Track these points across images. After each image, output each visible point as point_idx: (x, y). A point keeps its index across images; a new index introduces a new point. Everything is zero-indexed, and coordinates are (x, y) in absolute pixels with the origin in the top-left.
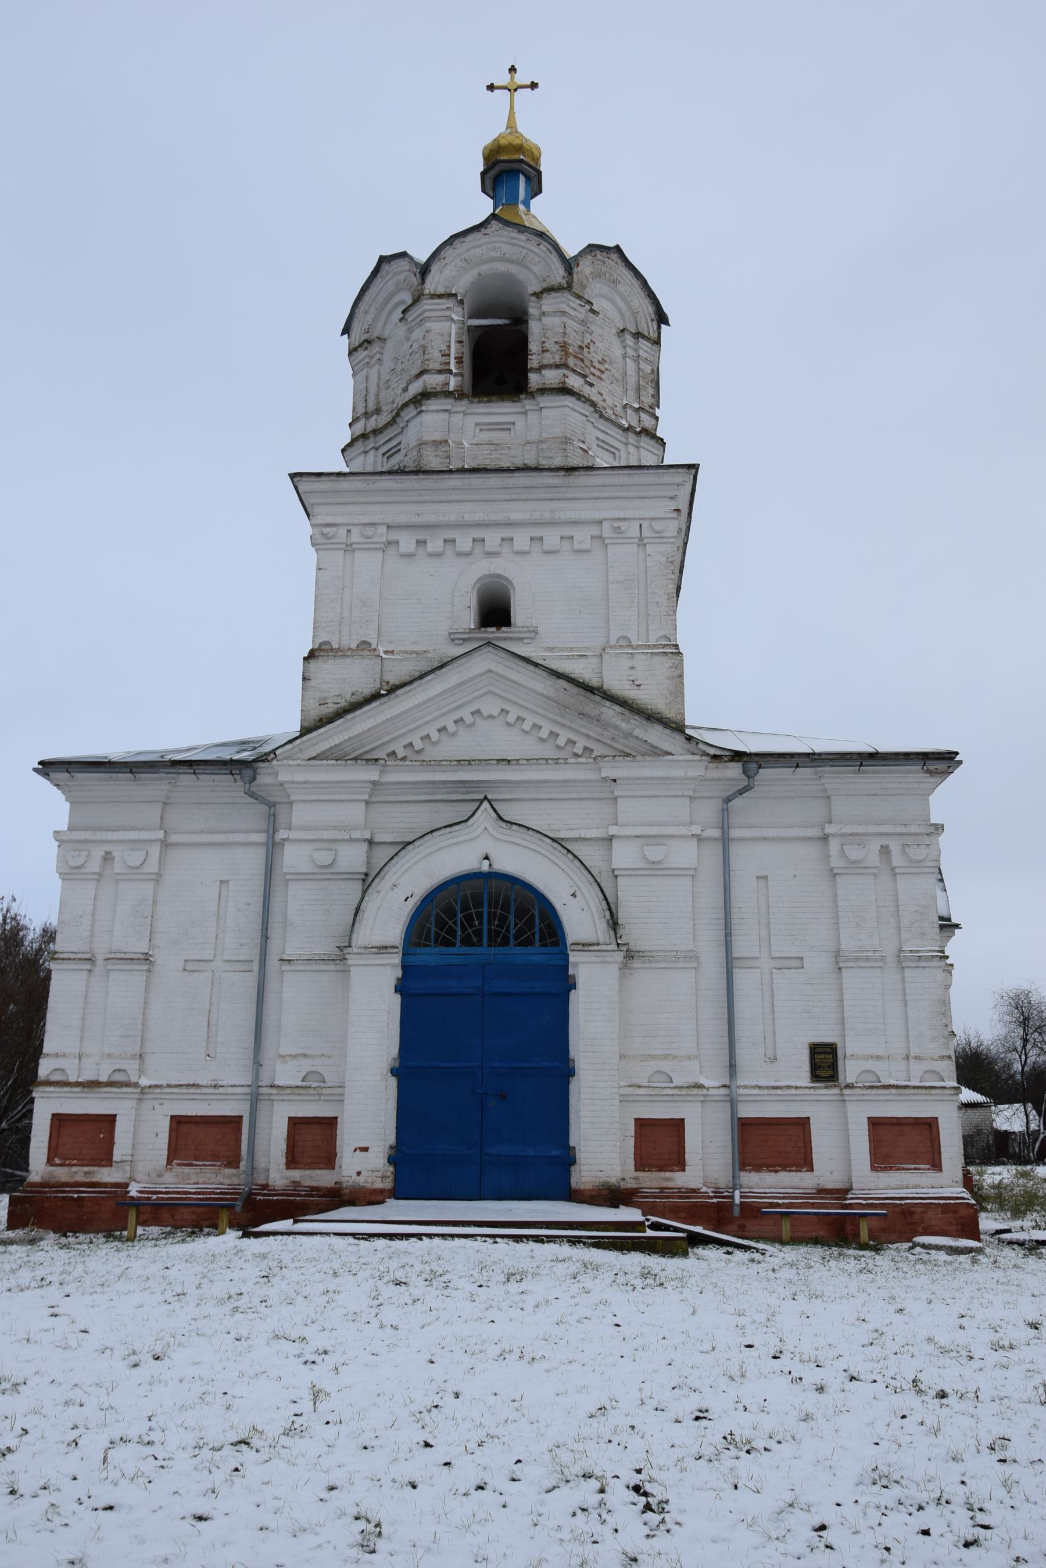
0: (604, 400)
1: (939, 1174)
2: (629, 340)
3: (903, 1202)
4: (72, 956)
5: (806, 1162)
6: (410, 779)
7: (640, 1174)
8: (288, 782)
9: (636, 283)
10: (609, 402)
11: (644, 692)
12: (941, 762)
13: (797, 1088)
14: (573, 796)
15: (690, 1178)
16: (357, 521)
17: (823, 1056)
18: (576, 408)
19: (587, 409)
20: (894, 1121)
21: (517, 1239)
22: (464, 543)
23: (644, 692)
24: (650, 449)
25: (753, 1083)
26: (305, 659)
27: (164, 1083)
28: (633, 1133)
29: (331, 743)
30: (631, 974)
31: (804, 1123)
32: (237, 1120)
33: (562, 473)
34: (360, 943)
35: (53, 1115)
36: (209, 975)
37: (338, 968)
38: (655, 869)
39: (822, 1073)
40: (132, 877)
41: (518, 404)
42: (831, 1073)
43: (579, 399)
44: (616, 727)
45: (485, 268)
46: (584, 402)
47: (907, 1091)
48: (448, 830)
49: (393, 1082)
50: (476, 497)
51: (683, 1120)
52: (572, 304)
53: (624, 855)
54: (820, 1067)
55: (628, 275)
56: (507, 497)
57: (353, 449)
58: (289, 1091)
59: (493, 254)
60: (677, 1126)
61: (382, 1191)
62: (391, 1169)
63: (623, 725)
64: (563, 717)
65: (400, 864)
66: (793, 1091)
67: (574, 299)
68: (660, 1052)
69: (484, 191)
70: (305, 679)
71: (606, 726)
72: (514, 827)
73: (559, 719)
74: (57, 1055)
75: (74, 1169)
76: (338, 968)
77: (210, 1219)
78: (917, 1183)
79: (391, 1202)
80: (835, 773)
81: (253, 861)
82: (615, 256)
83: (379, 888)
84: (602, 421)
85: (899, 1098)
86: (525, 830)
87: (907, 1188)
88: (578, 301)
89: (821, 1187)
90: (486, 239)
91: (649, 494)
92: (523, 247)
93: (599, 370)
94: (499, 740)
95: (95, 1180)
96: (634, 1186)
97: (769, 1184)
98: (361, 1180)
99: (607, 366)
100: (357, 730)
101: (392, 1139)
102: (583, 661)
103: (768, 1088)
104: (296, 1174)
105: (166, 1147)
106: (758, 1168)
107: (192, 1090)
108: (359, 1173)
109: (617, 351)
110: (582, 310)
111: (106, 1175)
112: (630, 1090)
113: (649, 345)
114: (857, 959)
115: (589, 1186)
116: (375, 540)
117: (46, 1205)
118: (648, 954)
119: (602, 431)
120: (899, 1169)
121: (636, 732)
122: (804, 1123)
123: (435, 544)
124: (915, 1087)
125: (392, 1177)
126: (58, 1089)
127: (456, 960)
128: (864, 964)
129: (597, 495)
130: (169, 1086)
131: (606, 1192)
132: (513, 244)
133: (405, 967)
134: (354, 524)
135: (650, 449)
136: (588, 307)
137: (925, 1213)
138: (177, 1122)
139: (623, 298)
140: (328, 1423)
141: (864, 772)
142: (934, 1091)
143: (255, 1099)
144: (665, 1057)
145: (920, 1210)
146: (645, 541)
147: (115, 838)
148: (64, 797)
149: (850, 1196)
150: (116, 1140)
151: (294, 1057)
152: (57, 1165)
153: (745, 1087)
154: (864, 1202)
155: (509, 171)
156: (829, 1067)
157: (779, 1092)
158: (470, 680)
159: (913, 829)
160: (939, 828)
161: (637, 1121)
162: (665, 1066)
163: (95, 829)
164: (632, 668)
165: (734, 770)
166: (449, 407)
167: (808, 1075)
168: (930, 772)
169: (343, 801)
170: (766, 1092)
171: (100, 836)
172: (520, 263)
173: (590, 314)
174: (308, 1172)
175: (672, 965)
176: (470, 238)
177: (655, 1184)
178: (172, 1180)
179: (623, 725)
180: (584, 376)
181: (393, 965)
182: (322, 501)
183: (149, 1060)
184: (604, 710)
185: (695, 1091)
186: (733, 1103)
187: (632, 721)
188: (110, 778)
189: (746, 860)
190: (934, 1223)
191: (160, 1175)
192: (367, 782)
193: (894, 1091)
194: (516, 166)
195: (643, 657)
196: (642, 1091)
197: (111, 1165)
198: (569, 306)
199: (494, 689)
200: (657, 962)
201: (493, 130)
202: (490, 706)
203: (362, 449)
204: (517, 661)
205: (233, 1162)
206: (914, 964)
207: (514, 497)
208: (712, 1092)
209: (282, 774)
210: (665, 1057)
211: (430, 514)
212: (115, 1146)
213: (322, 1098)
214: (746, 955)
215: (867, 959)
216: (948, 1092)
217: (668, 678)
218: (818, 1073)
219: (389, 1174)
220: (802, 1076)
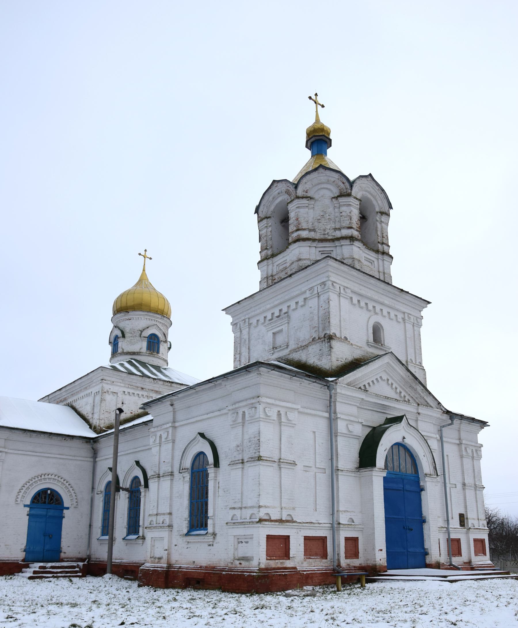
4: (268, 459)
12: (483, 424)
32: (323, 540)
37: (355, 475)
40: (287, 424)
41: (377, 255)
44: (420, 394)
51: (289, 536)
56: (383, 293)
58: (346, 526)
64: (404, 386)
74: (266, 507)
75: (277, 561)
76: (355, 475)
81: (322, 425)
95: (284, 566)
98: (381, 562)
104: (348, 561)
111: (288, 564)
115: (434, 563)
117: (274, 578)
121: (425, 397)
126: (270, 523)
129: (404, 302)
132: (373, 188)
143: (332, 528)
150: (291, 547)
151: (345, 511)
155: (318, 140)
160: (482, 446)
167: (459, 524)
169: (351, 404)
171: (278, 403)
178: (307, 565)
182: (333, 271)
188: (281, 376)
191: (302, 563)
192: (360, 398)
197: (289, 559)
203: (310, 245)
205: (325, 556)
211: (364, 291)
212: (291, 550)
213: (355, 529)
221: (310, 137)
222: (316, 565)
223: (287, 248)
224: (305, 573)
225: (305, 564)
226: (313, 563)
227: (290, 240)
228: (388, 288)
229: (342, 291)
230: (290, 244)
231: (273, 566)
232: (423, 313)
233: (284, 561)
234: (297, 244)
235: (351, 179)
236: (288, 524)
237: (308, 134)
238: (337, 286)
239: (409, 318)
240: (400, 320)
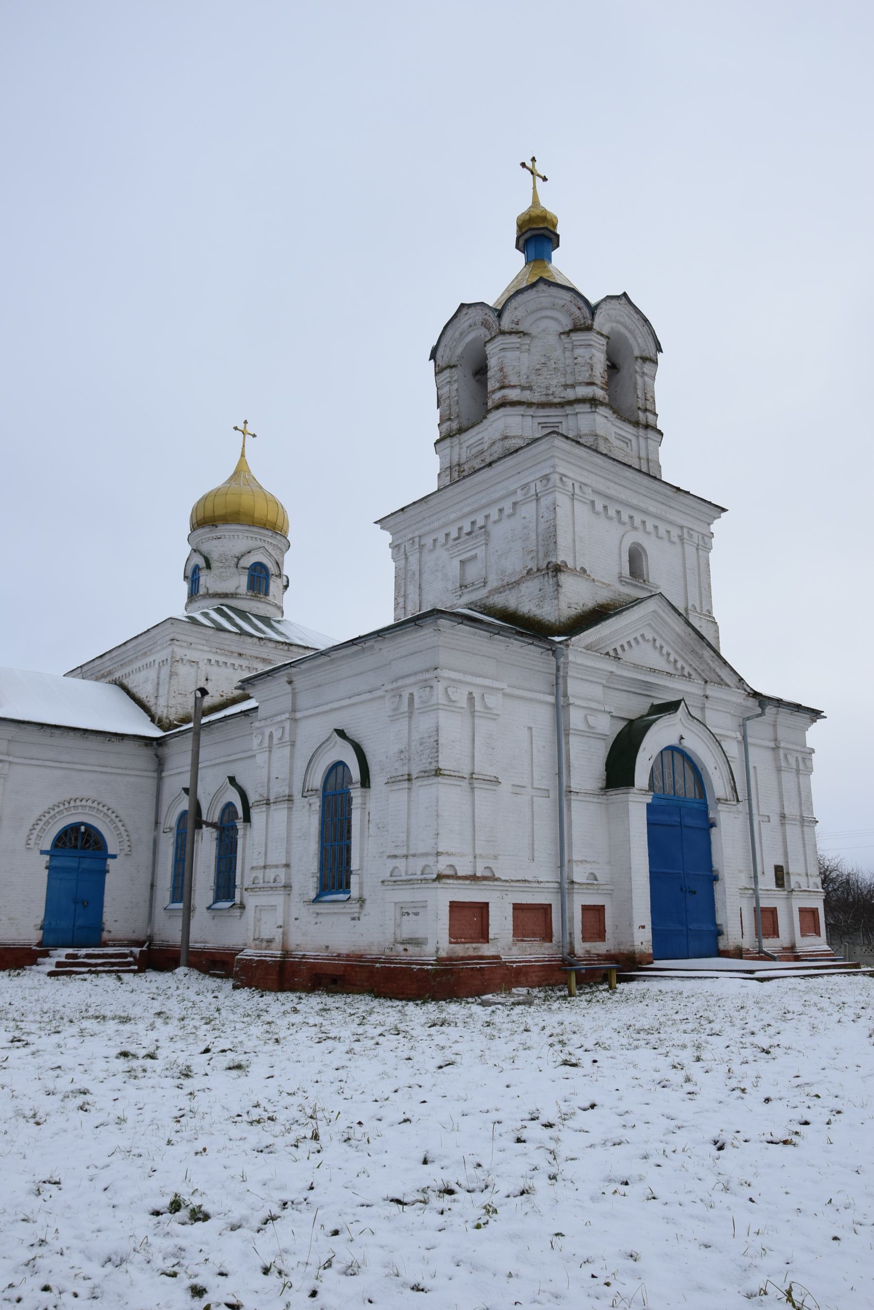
4: (452, 773)
8: (573, 663)
12: (815, 714)
32: (546, 909)
37: (599, 801)
41: (636, 429)
44: (708, 664)
51: (487, 904)
56: (646, 493)
57: (497, 412)
58: (584, 886)
69: (517, 247)
74: (448, 854)
75: (467, 946)
76: (599, 801)
77: (546, 980)
81: (544, 716)
95: (480, 954)
98: (643, 947)
104: (588, 945)
111: (487, 950)
121: (717, 670)
126: (455, 882)
130: (512, 881)
132: (629, 318)
140: (767, 1100)
147: (478, 682)
150: (490, 922)
160: (813, 751)
161: (487, 904)
163: (473, 674)
165: (752, 702)
169: (591, 681)
171: (468, 678)
172: (630, 331)
174: (593, 944)
181: (153, 777)
182: (561, 456)
188: (475, 634)
191: (510, 949)
197: (488, 942)
201: (523, 206)
205: (548, 936)
211: (614, 490)
224: (514, 965)
226: (528, 949)
231: (461, 954)
233: (479, 945)
236: (485, 882)
238: (569, 483)
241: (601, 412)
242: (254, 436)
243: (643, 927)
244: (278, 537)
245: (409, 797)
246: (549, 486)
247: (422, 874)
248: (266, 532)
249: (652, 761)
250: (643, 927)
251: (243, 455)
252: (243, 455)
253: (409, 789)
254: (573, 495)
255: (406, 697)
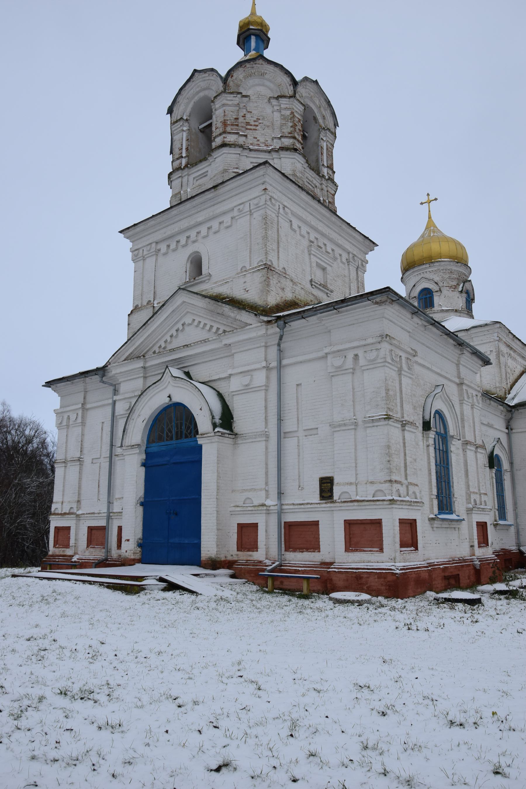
0: (258, 140)
1: (381, 554)
2: (274, 102)
3: (357, 571)
5: (315, 547)
6: (162, 361)
7: (239, 553)
9: (277, 70)
10: (262, 140)
11: (250, 294)
13: (312, 504)
14: (218, 357)
15: (259, 555)
16: (144, 245)
17: (325, 485)
18: (230, 152)
19: (238, 150)
20: (359, 522)
21: (90, 583)
22: (183, 240)
23: (250, 294)
24: (288, 156)
25: (291, 502)
26: (129, 315)
27: (85, 513)
28: (236, 531)
29: (130, 351)
30: (238, 447)
31: (316, 524)
33: (213, 190)
34: (126, 445)
35: (55, 527)
36: (98, 464)
38: (247, 389)
39: (325, 495)
41: (207, 161)
42: (330, 494)
43: (231, 147)
45: (196, 98)
46: (235, 147)
47: (363, 503)
48: (155, 385)
49: (140, 509)
50: (185, 216)
51: (318, 521)
52: (228, 98)
53: (235, 384)
54: (324, 491)
55: (271, 67)
59: (198, 90)
60: (255, 526)
61: (134, 560)
62: (139, 549)
63: (232, 315)
65: (140, 405)
66: (309, 506)
67: (229, 95)
68: (249, 488)
70: (129, 324)
71: (228, 317)
72: (177, 379)
73: (212, 318)
75: (60, 549)
78: (369, 559)
79: (139, 566)
80: (327, 316)
82: (261, 61)
83: (133, 418)
84: (253, 153)
85: (360, 508)
86: (181, 380)
87: (364, 562)
88: (232, 95)
89: (323, 561)
90: (194, 84)
91: (252, 186)
92: (209, 80)
93: (254, 125)
94: (193, 334)
96: (236, 559)
97: (298, 559)
98: (127, 554)
99: (260, 121)
100: (137, 344)
101: (140, 535)
102: (227, 284)
103: (298, 504)
105: (86, 540)
106: (295, 550)
107: (92, 515)
108: (126, 551)
109: (268, 110)
110: (237, 99)
112: (234, 509)
113: (287, 100)
114: (340, 426)
116: (151, 251)
118: (245, 435)
119: (257, 158)
120: (361, 551)
122: (316, 524)
123: (173, 246)
124: (368, 501)
125: (140, 553)
127: (163, 448)
128: (344, 428)
131: (210, 562)
132: (204, 80)
133: (147, 453)
134: (144, 246)
135: (288, 156)
136: (239, 96)
137: (368, 578)
138: (349, 524)
139: (270, 81)
141: (342, 312)
142: (378, 503)
143: (109, 518)
144: (251, 490)
145: (365, 576)
146: (252, 211)
148: (57, 395)
149: (332, 566)
152: (57, 548)
153: (287, 504)
154: (337, 570)
156: (329, 491)
157: (302, 506)
158: (176, 308)
159: (370, 341)
162: (250, 495)
164: (245, 282)
166: (180, 175)
168: (377, 303)
170: (296, 507)
173: (244, 99)
175: (254, 440)
176: (187, 87)
177: (245, 558)
178: (88, 554)
179: (232, 315)
180: (238, 133)
183: (83, 503)
184: (224, 309)
185: (261, 508)
186: (280, 513)
187: (235, 312)
189: (291, 376)
190: (373, 584)
191: (85, 552)
193: (356, 504)
194: (247, 33)
195: (249, 275)
196: (239, 509)
198: (227, 100)
199: (189, 311)
200: (248, 439)
202: (188, 320)
204: (193, 294)
206: (371, 425)
207: (199, 210)
208: (272, 508)
209: (114, 371)
210: (251, 490)
214: (291, 430)
215: (345, 425)
216: (385, 503)
217: (260, 283)
218: (323, 494)
219: (138, 552)
220: (315, 497)
221: (243, 30)
222: (98, 554)
223: (210, 155)
224: (441, 567)
225: (87, 553)
226: (94, 553)
227: (214, 147)
228: (334, 218)
229: (281, 211)
230: (212, 150)
231: (57, 553)
232: (368, 257)
233: (65, 549)
234: (225, 150)
235: (298, 78)
236: (67, 516)
237: (241, 28)
238: (277, 204)
239: (354, 260)
240: (344, 260)
241: (174, 178)
242: (422, 204)
243: (128, 540)
244: (436, 264)
245: (65, 471)
246: (151, 251)
247: (244, 504)
248: (424, 266)
249: (145, 422)
250: (128, 540)
251: (430, 217)
252: (430, 217)
253: (65, 467)
254: (278, 213)
255: (66, 417)
